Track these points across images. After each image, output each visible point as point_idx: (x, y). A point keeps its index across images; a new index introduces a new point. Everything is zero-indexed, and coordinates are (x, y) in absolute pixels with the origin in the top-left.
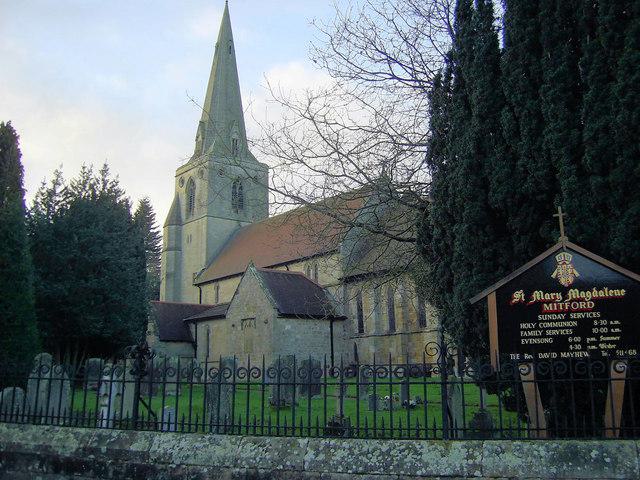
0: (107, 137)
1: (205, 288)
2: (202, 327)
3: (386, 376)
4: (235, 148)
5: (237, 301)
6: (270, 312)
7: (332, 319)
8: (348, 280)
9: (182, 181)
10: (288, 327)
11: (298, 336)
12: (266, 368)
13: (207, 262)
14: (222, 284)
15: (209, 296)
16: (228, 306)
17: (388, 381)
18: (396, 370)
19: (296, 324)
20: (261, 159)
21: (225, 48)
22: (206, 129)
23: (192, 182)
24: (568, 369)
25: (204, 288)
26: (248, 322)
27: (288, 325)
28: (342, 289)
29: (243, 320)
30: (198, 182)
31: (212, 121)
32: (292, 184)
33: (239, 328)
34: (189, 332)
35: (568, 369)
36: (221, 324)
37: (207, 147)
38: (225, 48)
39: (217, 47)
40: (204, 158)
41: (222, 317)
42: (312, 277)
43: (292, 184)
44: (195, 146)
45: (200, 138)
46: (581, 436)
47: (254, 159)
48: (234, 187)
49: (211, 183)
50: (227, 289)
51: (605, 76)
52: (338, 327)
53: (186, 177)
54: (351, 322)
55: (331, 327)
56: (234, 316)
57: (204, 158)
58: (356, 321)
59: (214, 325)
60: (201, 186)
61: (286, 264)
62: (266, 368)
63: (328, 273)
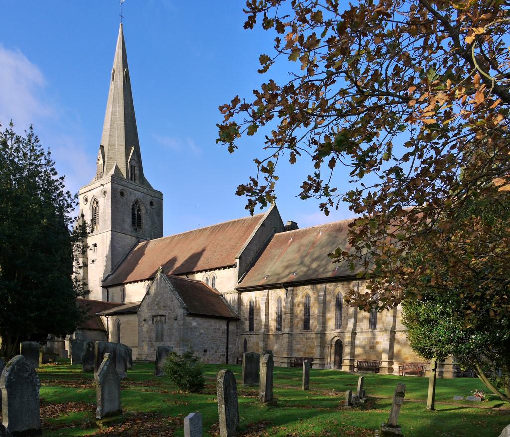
6: (180, 312)
7: (229, 320)
10: (194, 324)
11: (202, 331)
13: (112, 269)
23: (96, 201)
25: (110, 290)
26: (159, 318)
27: (194, 322)
28: (237, 294)
29: (154, 316)
30: (101, 201)
34: (102, 324)
36: (133, 318)
38: (203, 250)
42: (210, 285)
46: (109, 89)
47: (150, 186)
48: (133, 209)
51: (376, 280)
52: (232, 327)
54: (243, 323)
55: (227, 326)
58: (247, 323)
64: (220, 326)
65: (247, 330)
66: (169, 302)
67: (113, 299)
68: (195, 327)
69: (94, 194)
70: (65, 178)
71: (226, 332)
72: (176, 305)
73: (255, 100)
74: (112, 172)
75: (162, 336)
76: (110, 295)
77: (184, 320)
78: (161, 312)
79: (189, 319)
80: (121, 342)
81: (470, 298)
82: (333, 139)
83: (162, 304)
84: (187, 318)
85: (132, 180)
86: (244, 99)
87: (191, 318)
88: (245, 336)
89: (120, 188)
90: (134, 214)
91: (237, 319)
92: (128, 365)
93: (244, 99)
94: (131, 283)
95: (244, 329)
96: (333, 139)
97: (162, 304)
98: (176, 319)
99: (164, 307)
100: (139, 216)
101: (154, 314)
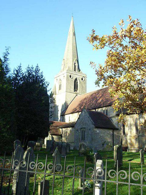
10: (98, 131)
26: (83, 129)
55: (113, 132)
66: (87, 122)
68: (98, 133)
69: (120, 131)
70: (38, 65)
71: (112, 135)
72: (90, 123)
74: (67, 68)
75: (84, 138)
78: (84, 127)
79: (96, 130)
82: (83, 149)
83: (84, 123)
85: (75, 71)
87: (96, 129)
90: (75, 84)
92: (68, 151)
94: (67, 114)
96: (83, 149)
97: (84, 123)
99: (85, 124)
100: (77, 85)
101: (81, 127)
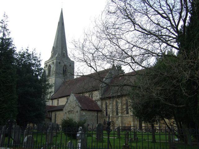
0: (33, 42)
1: (54, 101)
2: (53, 114)
3: (158, 132)
4: (64, 55)
5: (67, 105)
6: (78, 109)
8: (102, 99)
9: (47, 66)
10: (84, 113)
11: (87, 117)
12: (93, 128)
14: (60, 100)
15: (55, 103)
16: (64, 106)
17: (113, 133)
18: (158, 131)
19: (91, 113)
20: (72, 59)
21: (61, 24)
22: (54, 50)
23: (50, 66)
24: (196, 131)
30: (52, 66)
31: (57, 46)
32: (81, 69)
33: (68, 114)
35: (196, 131)
36: (61, 112)
37: (55, 55)
38: (61, 24)
39: (59, 23)
40: (54, 58)
41: (62, 110)
43: (81, 69)
44: (51, 55)
45: (53, 52)
49: (57, 65)
50: (62, 102)
52: (99, 114)
53: (48, 64)
55: (97, 114)
56: (65, 110)
57: (54, 58)
58: (105, 112)
59: (58, 113)
60: (53, 68)
61: (83, 93)
62: (93, 128)
63: (96, 96)
64: (94, 114)
65: (105, 115)
67: (54, 104)
68: (84, 115)
73: (37, 54)
76: (53, 103)
77: (80, 112)
80: (56, 122)
81: (179, 65)
84: (81, 111)
86: (40, 54)
88: (105, 118)
89: (59, 61)
91: (101, 111)
93: (40, 54)
95: (104, 115)
98: (77, 112)
